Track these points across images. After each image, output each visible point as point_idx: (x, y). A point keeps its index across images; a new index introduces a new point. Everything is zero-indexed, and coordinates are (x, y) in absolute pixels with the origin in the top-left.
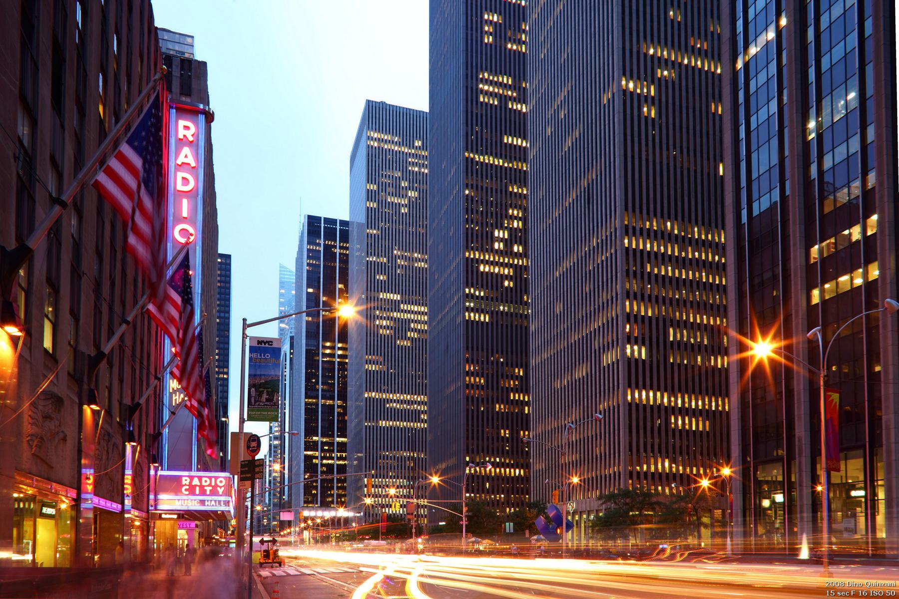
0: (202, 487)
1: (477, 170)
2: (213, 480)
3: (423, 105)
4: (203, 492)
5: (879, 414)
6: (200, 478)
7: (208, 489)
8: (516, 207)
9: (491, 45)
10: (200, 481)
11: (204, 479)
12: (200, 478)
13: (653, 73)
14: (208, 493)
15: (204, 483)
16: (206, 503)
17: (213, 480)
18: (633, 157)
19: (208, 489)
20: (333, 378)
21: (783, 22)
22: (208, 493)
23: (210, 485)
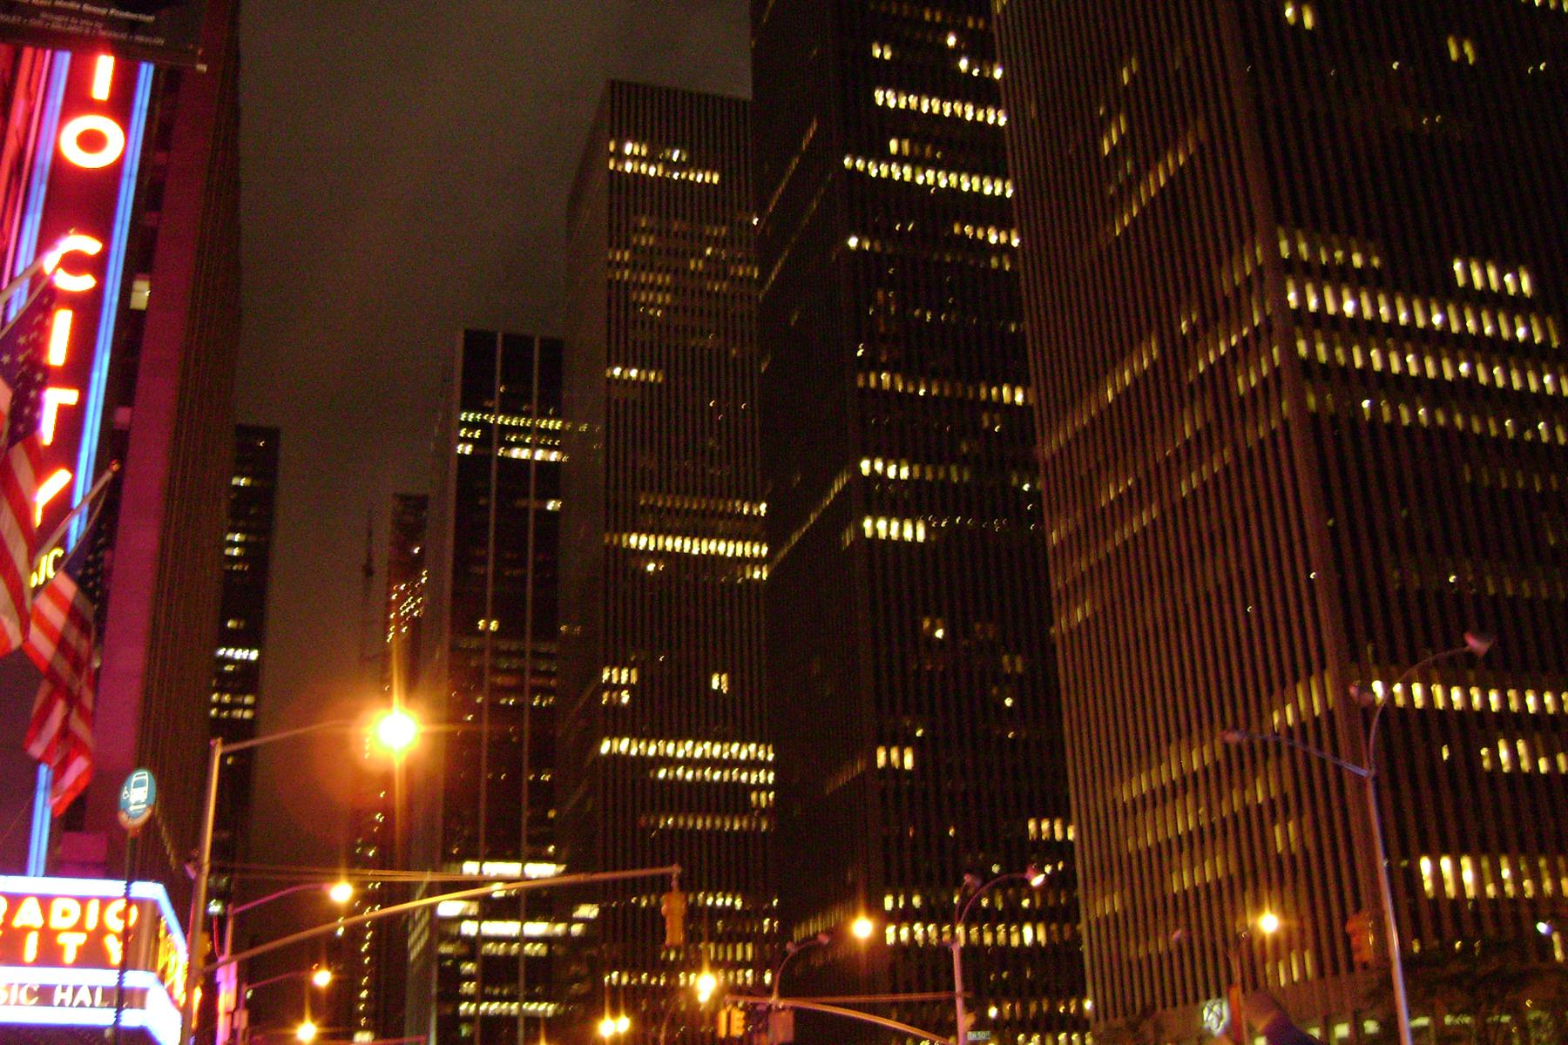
0: (48, 936)
1: (1405, 504)
2: (93, 907)
3: (744, 90)
4: (50, 955)
5: (969, 995)
6: (45, 901)
7: (71, 944)
8: (741, 279)
9: (660, 386)
10: (46, 912)
11: (57, 906)
12: (45, 901)
13: (628, 240)
14: (70, 956)
15: (55, 923)
16: (58, 996)
17: (93, 907)
18: (1230, 679)
19: (71, 944)
20: (522, 563)
21: (1194, 318)
22: (70, 956)
23: (79, 927)
